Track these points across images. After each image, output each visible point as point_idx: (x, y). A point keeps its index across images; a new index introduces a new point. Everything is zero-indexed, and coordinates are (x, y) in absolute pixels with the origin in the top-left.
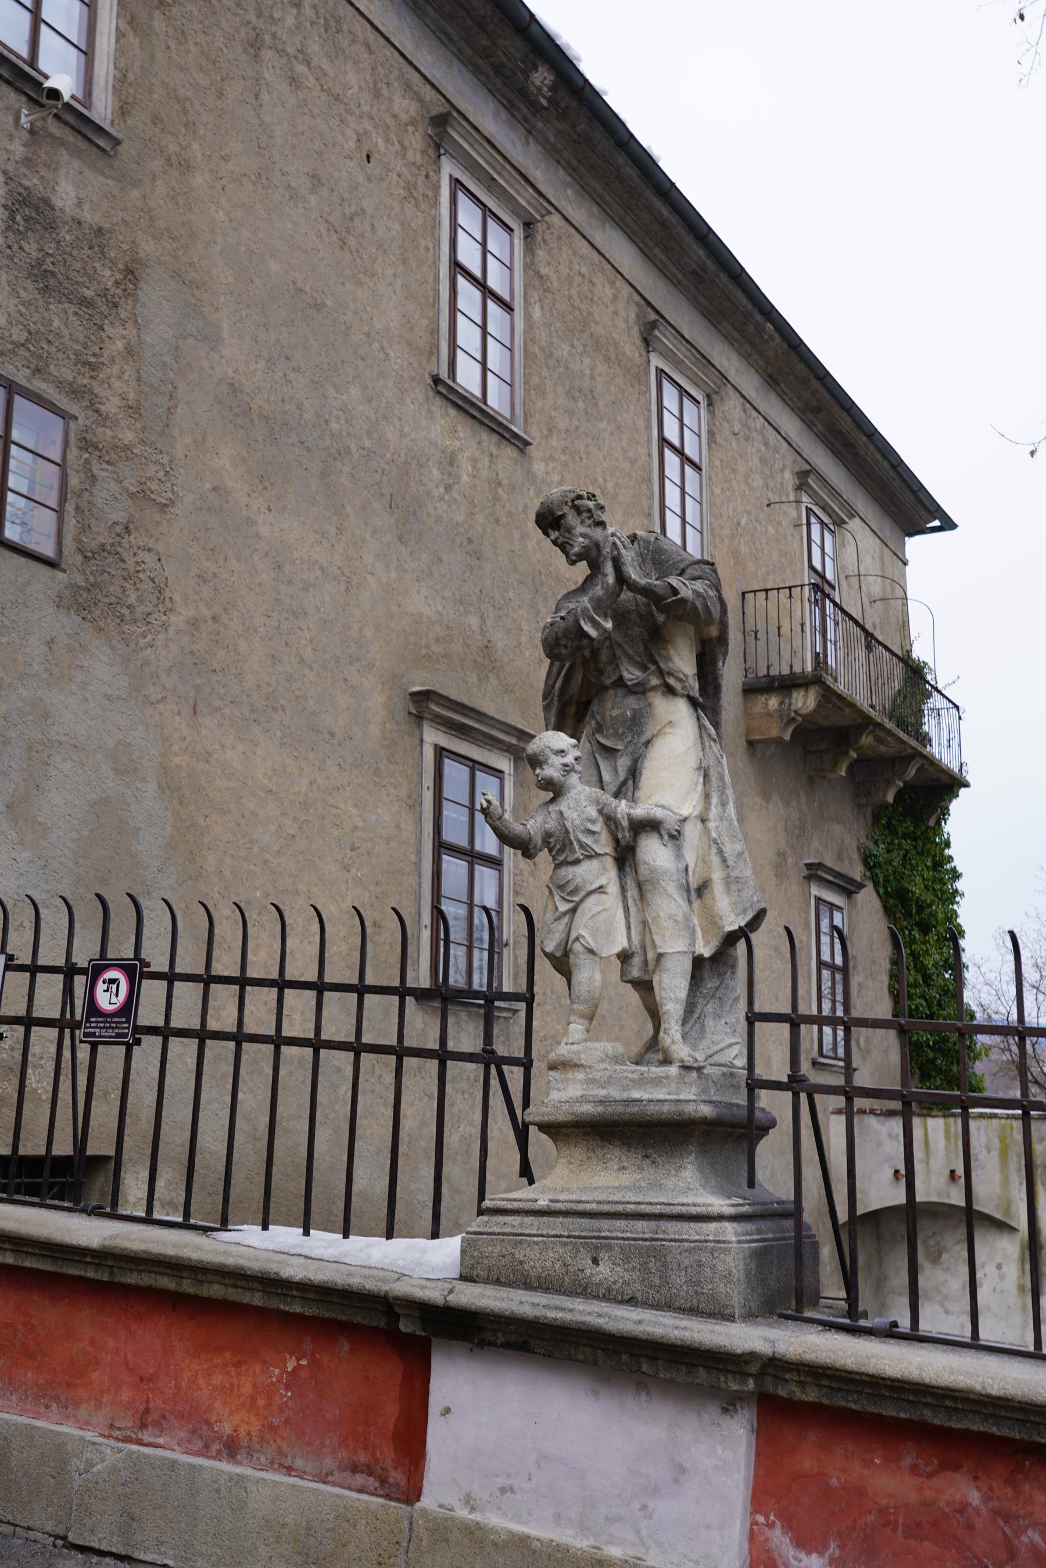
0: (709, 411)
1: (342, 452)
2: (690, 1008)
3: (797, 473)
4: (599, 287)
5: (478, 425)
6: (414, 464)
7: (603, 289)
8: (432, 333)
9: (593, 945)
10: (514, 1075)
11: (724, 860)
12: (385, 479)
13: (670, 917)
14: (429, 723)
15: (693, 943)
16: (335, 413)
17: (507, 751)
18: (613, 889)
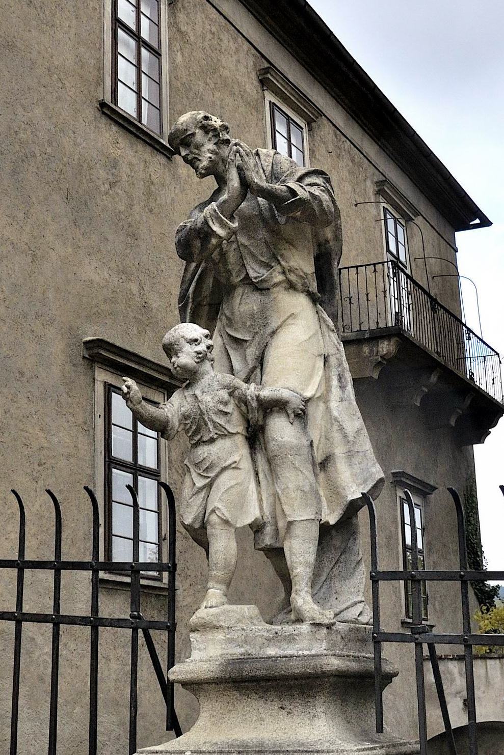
0: (309, 135)
2: (316, 575)
3: (376, 182)
4: (225, 41)
5: (135, 139)
6: (85, 165)
7: (228, 41)
8: (99, 70)
9: (228, 516)
10: (160, 638)
12: (62, 176)
13: (298, 488)
14: (100, 365)
15: (319, 512)
16: (23, 126)
18: (246, 464)
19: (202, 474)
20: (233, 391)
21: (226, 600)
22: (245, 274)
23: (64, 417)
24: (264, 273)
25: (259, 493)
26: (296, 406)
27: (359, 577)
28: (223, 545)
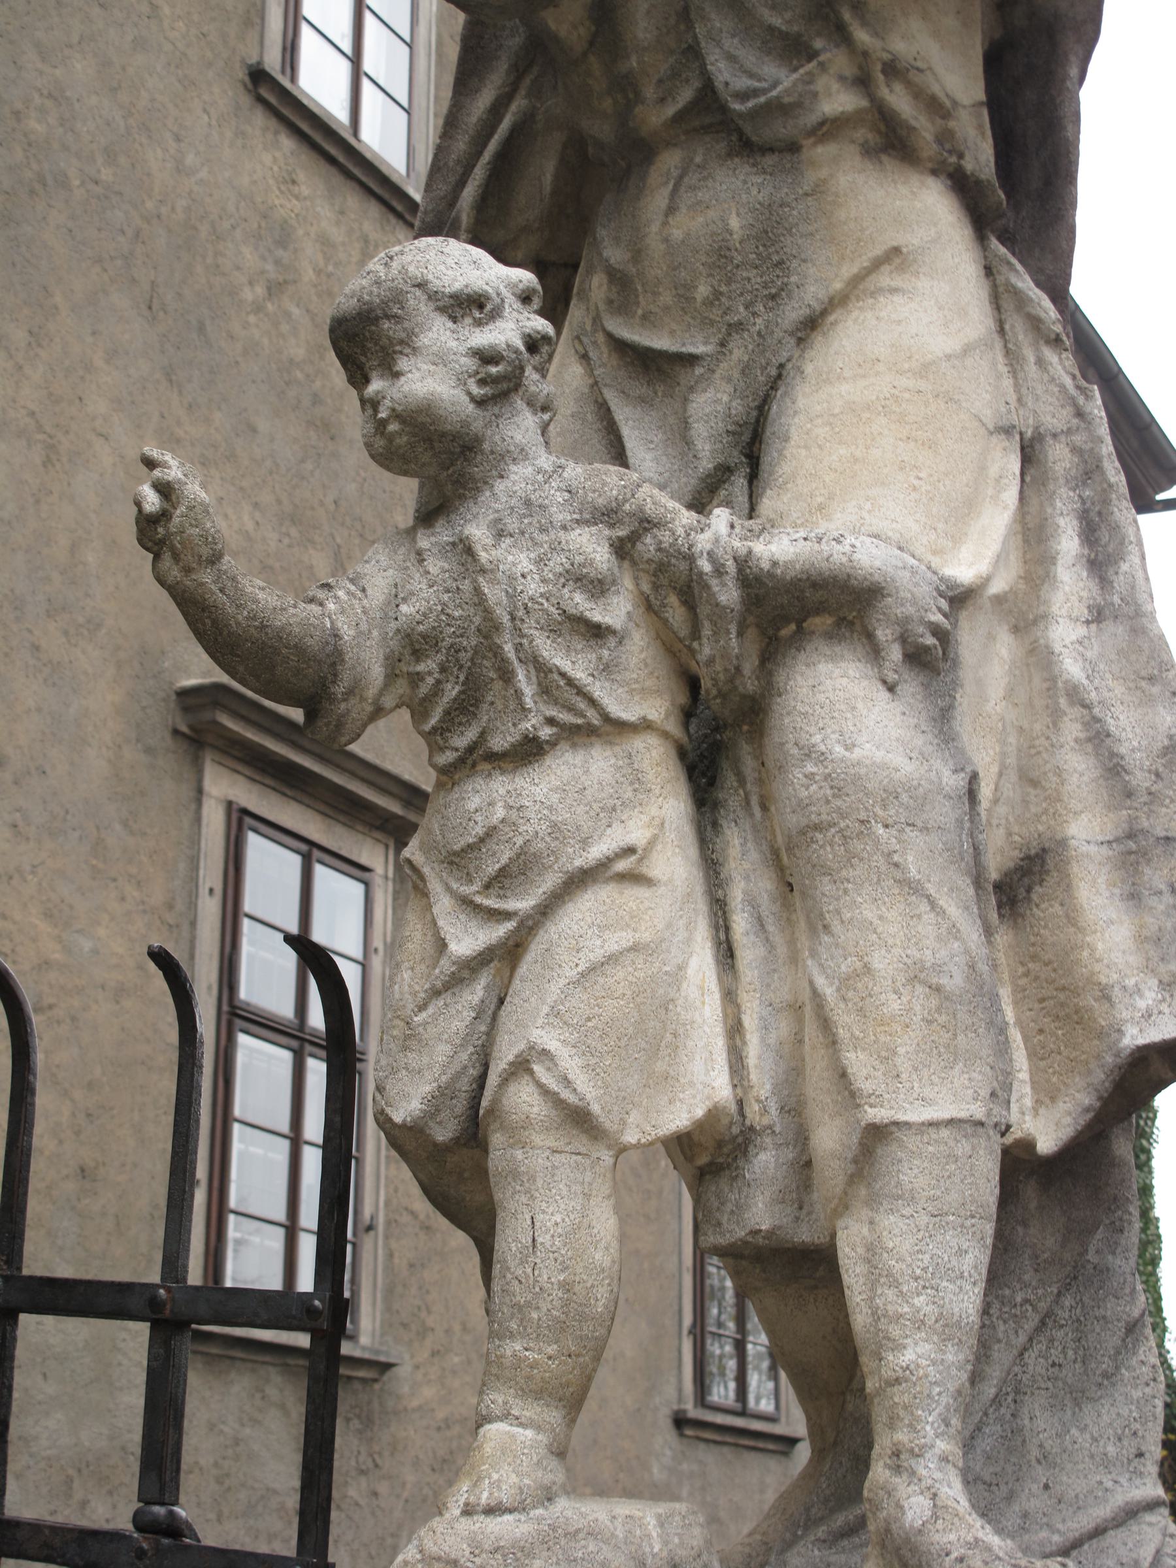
1: (50, 181)
6: (204, 229)
9: (587, 1089)
11: (1114, 769)
13: (916, 975)
15: (1000, 1094)
16: (37, 100)
17: (381, 828)
18: (675, 865)
19: (478, 899)
20: (635, 537)
21: (561, 1477)
22: (697, 84)
23: (112, 885)
24: (781, 79)
25: (730, 996)
26: (910, 610)
27: (1136, 1394)
28: (567, 1219)
